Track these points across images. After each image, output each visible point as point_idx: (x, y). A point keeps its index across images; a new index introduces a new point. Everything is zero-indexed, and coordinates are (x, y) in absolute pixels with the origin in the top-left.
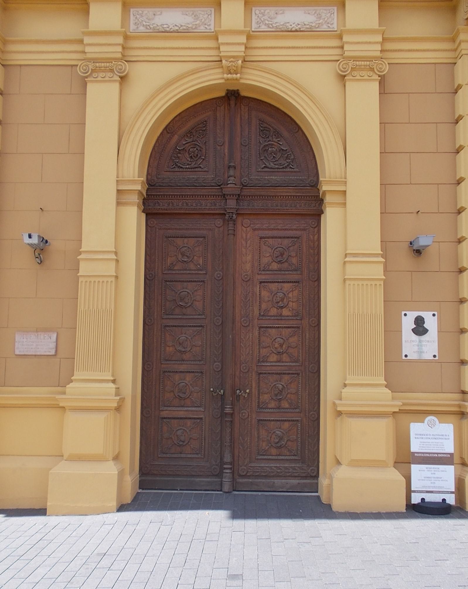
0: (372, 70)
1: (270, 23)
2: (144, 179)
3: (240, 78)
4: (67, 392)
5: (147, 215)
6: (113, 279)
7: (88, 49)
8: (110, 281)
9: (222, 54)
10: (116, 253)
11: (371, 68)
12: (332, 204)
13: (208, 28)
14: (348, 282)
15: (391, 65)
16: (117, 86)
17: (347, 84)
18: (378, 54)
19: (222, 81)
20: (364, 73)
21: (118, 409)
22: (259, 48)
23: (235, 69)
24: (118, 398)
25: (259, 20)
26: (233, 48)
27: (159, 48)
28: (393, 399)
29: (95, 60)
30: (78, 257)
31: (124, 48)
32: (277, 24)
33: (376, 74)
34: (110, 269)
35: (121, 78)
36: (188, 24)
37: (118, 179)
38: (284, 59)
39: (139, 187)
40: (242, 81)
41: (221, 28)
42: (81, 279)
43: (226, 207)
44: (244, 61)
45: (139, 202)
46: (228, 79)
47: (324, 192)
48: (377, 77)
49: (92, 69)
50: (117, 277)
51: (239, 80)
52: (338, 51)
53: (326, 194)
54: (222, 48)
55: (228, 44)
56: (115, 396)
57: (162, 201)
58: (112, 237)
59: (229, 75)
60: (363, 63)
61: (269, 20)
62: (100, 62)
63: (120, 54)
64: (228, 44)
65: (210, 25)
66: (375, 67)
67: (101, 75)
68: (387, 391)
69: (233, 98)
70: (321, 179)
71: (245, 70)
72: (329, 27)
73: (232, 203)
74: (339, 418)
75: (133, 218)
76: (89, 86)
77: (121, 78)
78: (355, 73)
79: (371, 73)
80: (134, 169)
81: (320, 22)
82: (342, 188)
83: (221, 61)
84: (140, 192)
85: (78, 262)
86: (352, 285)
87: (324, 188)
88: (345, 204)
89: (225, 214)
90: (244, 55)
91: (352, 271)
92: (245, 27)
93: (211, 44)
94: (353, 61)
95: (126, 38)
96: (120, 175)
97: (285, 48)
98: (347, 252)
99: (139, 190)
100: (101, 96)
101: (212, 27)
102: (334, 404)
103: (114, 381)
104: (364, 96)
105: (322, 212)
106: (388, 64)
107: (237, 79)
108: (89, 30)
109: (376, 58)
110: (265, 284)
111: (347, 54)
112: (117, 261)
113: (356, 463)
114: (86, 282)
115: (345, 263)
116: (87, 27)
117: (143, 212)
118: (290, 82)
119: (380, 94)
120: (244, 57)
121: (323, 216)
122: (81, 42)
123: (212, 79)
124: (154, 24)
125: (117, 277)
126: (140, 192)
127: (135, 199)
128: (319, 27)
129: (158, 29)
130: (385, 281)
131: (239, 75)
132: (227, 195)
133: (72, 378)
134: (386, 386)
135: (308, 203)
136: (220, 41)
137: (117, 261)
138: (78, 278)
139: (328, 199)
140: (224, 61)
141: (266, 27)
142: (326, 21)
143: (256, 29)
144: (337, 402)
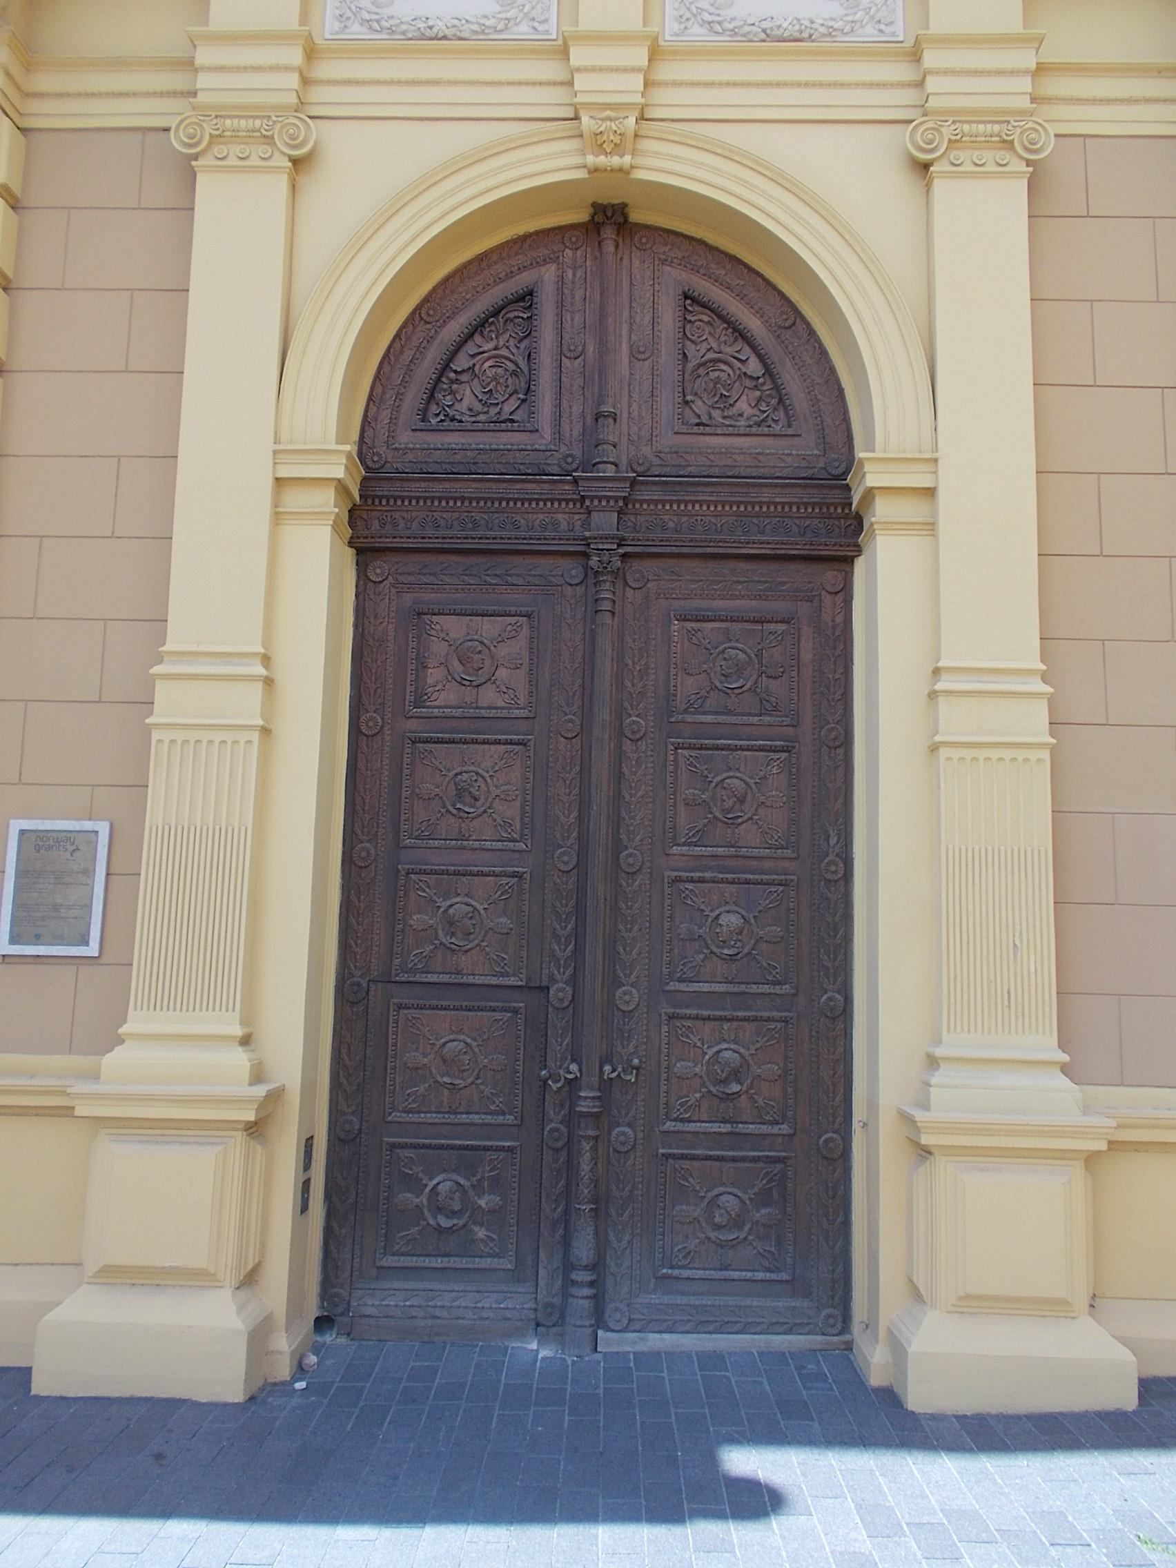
0: (1009, 145)
1: (374, 17)
2: (351, 448)
3: (632, 167)
4: (102, 1077)
5: (360, 551)
6: (255, 737)
7: (203, 81)
8: (179, 740)
9: (580, 99)
10: (266, 660)
11: (1004, 141)
12: (890, 526)
13: (541, 28)
14: (944, 753)
15: (1061, 139)
16: (282, 183)
17: (938, 185)
18: (1025, 103)
19: (581, 174)
20: (988, 156)
21: (255, 1129)
22: (674, 84)
23: (617, 140)
24: (260, 1091)
25: (683, 10)
26: (609, 80)
27: (748, 85)
28: (1086, 1110)
29: (221, 111)
30: (151, 671)
31: (306, 81)
32: (391, 22)
33: (282, 152)
34: (245, 704)
35: (296, 162)
36: (485, 17)
37: (278, 447)
38: (739, 117)
39: (339, 472)
40: (640, 175)
41: (928, 28)
42: (156, 735)
43: (587, 534)
44: (642, 118)
45: (337, 514)
46: (595, 170)
47: (870, 494)
48: (1022, 167)
49: (950, 141)
50: (266, 731)
51: (628, 173)
52: (909, 96)
53: (873, 499)
54: (580, 82)
55: (592, 69)
56: (251, 1084)
57: (404, 514)
58: (257, 615)
59: (602, 158)
60: (981, 127)
61: (712, 10)
62: (235, 117)
63: (294, 94)
64: (592, 69)
65: (545, 21)
66: (1016, 137)
67: (236, 149)
68: (1065, 1082)
69: (609, 222)
70: (860, 454)
71: (646, 145)
72: (881, 31)
73: (605, 521)
74: (922, 1169)
75: (317, 564)
76: (205, 184)
77: (296, 162)
78: (962, 156)
79: (1008, 156)
80: (321, 418)
81: (509, 15)
82: (924, 482)
83: (576, 118)
84: (341, 486)
85: (150, 683)
86: (242, 744)
87: (873, 478)
88: (930, 527)
89: (586, 556)
90: (643, 101)
91: (957, 720)
92: (1025, 28)
93: (550, 70)
94: (954, 122)
95: (311, 53)
96: (285, 436)
97: (821, 85)
98: (940, 664)
99: (339, 480)
100: (235, 214)
101: (552, 26)
102: (908, 1120)
103: (246, 1041)
104: (984, 218)
105: (859, 550)
106: (1056, 136)
107: (621, 170)
108: (580, 28)
109: (1022, 113)
110: (429, 746)
111: (933, 103)
112: (268, 682)
113: (974, 1304)
114: (186, 741)
115: (933, 695)
116: (204, 18)
117: (350, 544)
118: (784, 182)
119: (193, 209)
120: (643, 108)
121: (860, 565)
122: (188, 65)
123: (554, 164)
124: (733, 19)
125: (266, 731)
126: (341, 486)
127: (327, 502)
128: (506, 28)
129: (404, 33)
130: (1054, 750)
131: (627, 159)
132: (592, 498)
133: (121, 1031)
134: (1065, 1069)
135: (816, 527)
136: (574, 62)
137: (268, 682)
138: (148, 730)
139: (882, 510)
140: (585, 119)
141: (704, 31)
142: (526, 15)
143: (677, 35)
144: (919, 1115)
